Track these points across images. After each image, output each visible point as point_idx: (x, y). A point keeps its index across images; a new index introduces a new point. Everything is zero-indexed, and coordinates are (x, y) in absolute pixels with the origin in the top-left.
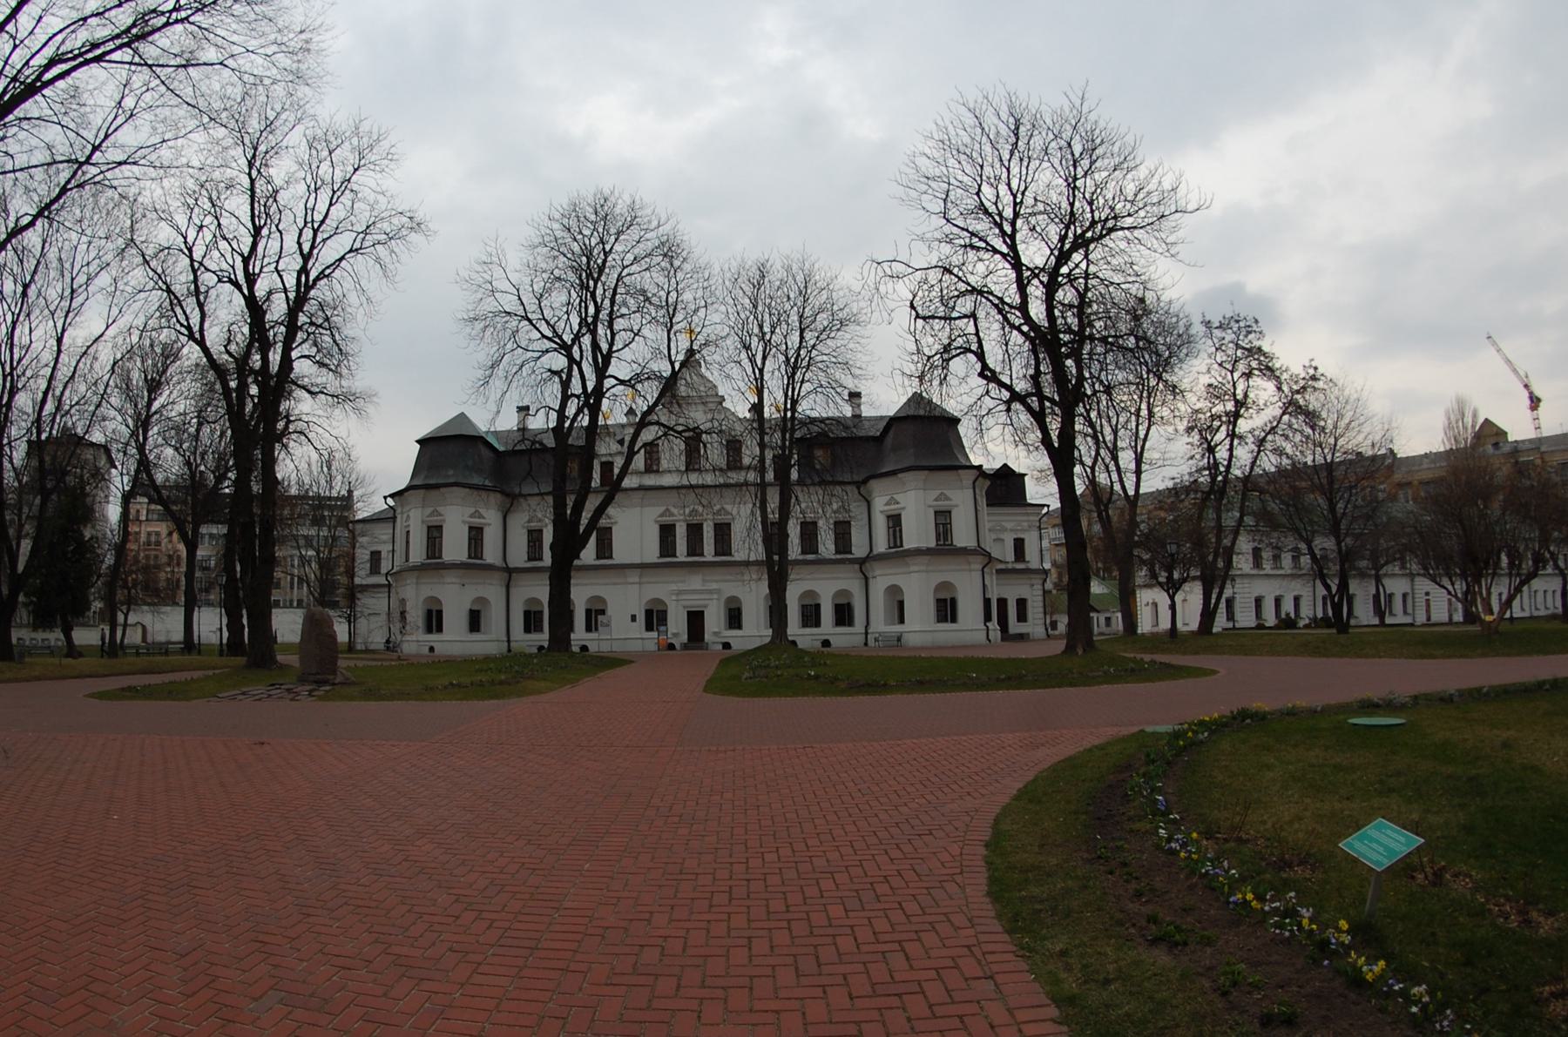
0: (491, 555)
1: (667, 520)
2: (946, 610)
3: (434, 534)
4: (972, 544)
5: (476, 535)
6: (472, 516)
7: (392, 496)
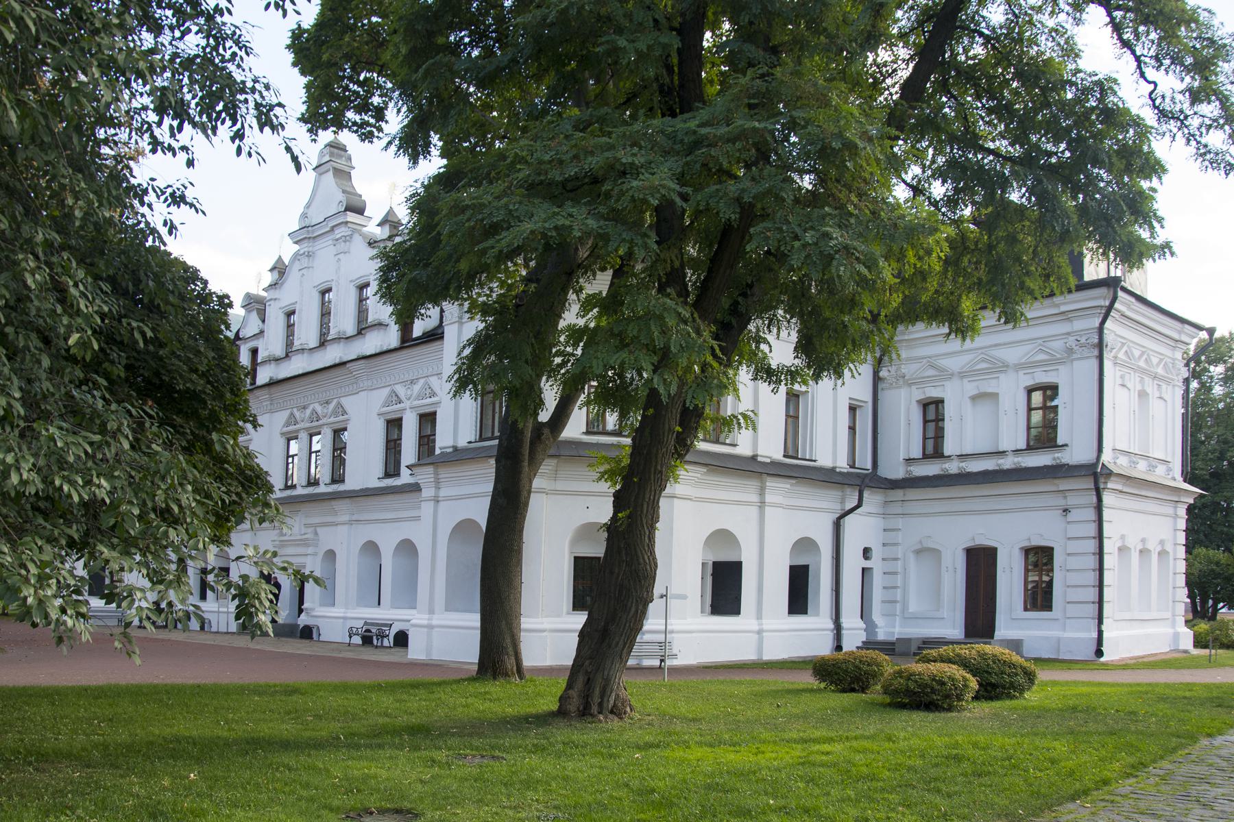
1: (393, 410)
6: (387, 404)
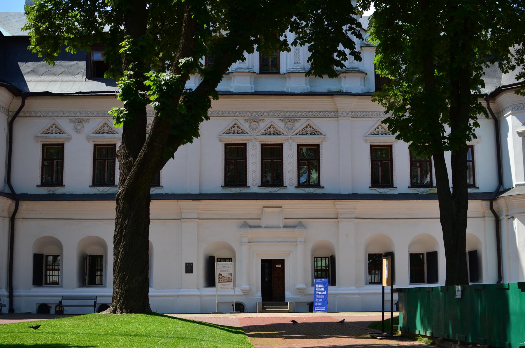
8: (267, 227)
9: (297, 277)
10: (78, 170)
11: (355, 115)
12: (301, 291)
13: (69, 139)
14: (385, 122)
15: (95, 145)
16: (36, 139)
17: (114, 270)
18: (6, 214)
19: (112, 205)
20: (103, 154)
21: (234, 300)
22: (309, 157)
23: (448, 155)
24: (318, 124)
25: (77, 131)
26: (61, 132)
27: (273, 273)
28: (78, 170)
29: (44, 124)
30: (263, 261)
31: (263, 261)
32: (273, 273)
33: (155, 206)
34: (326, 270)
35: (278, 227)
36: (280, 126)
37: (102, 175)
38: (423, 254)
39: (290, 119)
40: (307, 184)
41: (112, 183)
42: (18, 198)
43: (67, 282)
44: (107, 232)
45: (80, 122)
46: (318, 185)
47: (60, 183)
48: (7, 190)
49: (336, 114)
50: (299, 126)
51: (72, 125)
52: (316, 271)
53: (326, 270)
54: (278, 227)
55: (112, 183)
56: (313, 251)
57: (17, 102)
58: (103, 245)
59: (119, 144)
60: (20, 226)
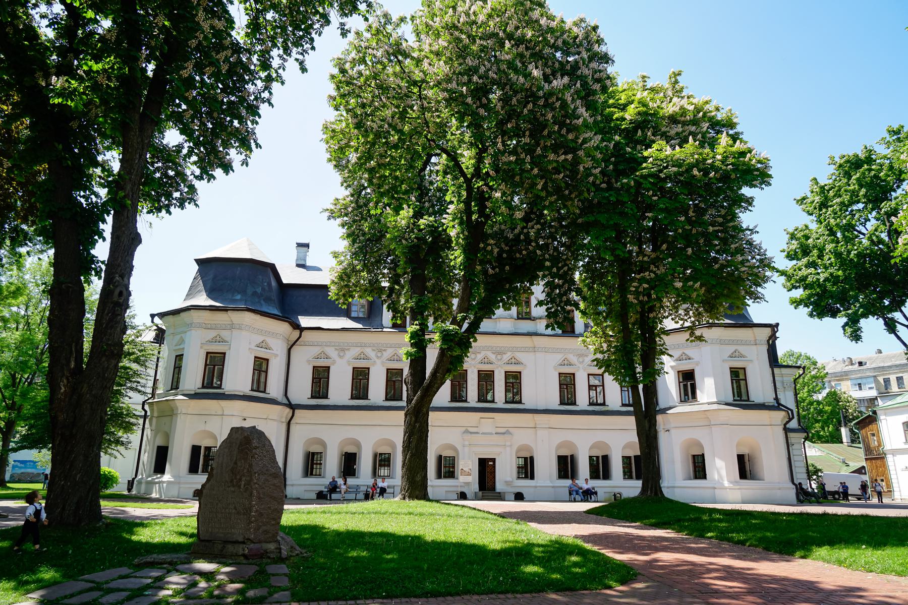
0: (274, 388)
2: (745, 468)
3: (215, 364)
4: (769, 399)
5: (261, 366)
7: (162, 315)
8: (483, 433)
9: (506, 474)
10: (377, 389)
11: (546, 350)
12: (508, 483)
13: (334, 362)
14: (593, 361)
15: (354, 368)
16: (308, 361)
17: (403, 467)
18: (284, 420)
19: (402, 414)
20: (393, 377)
21: (460, 490)
22: (514, 381)
23: (641, 387)
24: (520, 356)
25: (340, 357)
26: (368, 359)
27: (486, 467)
28: (377, 389)
29: (316, 351)
30: (480, 459)
31: (480, 459)
32: (486, 467)
33: (432, 416)
34: (527, 469)
35: (491, 434)
36: (492, 357)
37: (393, 393)
38: (567, 457)
39: (499, 352)
40: (513, 402)
41: (401, 400)
42: (293, 407)
43: (364, 475)
44: (397, 436)
45: (343, 350)
46: (520, 402)
47: (366, 397)
48: (285, 401)
49: (534, 349)
50: (506, 357)
51: (337, 352)
52: (321, 464)
53: (527, 469)
54: (491, 434)
55: (401, 400)
56: (517, 451)
57: (297, 333)
58: (393, 445)
59: (406, 372)
60: (293, 428)
